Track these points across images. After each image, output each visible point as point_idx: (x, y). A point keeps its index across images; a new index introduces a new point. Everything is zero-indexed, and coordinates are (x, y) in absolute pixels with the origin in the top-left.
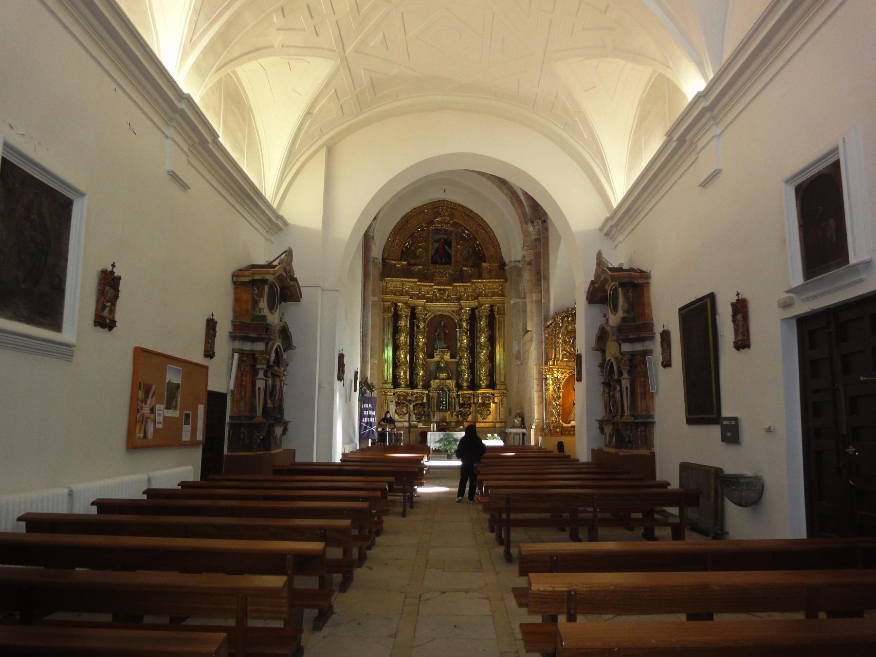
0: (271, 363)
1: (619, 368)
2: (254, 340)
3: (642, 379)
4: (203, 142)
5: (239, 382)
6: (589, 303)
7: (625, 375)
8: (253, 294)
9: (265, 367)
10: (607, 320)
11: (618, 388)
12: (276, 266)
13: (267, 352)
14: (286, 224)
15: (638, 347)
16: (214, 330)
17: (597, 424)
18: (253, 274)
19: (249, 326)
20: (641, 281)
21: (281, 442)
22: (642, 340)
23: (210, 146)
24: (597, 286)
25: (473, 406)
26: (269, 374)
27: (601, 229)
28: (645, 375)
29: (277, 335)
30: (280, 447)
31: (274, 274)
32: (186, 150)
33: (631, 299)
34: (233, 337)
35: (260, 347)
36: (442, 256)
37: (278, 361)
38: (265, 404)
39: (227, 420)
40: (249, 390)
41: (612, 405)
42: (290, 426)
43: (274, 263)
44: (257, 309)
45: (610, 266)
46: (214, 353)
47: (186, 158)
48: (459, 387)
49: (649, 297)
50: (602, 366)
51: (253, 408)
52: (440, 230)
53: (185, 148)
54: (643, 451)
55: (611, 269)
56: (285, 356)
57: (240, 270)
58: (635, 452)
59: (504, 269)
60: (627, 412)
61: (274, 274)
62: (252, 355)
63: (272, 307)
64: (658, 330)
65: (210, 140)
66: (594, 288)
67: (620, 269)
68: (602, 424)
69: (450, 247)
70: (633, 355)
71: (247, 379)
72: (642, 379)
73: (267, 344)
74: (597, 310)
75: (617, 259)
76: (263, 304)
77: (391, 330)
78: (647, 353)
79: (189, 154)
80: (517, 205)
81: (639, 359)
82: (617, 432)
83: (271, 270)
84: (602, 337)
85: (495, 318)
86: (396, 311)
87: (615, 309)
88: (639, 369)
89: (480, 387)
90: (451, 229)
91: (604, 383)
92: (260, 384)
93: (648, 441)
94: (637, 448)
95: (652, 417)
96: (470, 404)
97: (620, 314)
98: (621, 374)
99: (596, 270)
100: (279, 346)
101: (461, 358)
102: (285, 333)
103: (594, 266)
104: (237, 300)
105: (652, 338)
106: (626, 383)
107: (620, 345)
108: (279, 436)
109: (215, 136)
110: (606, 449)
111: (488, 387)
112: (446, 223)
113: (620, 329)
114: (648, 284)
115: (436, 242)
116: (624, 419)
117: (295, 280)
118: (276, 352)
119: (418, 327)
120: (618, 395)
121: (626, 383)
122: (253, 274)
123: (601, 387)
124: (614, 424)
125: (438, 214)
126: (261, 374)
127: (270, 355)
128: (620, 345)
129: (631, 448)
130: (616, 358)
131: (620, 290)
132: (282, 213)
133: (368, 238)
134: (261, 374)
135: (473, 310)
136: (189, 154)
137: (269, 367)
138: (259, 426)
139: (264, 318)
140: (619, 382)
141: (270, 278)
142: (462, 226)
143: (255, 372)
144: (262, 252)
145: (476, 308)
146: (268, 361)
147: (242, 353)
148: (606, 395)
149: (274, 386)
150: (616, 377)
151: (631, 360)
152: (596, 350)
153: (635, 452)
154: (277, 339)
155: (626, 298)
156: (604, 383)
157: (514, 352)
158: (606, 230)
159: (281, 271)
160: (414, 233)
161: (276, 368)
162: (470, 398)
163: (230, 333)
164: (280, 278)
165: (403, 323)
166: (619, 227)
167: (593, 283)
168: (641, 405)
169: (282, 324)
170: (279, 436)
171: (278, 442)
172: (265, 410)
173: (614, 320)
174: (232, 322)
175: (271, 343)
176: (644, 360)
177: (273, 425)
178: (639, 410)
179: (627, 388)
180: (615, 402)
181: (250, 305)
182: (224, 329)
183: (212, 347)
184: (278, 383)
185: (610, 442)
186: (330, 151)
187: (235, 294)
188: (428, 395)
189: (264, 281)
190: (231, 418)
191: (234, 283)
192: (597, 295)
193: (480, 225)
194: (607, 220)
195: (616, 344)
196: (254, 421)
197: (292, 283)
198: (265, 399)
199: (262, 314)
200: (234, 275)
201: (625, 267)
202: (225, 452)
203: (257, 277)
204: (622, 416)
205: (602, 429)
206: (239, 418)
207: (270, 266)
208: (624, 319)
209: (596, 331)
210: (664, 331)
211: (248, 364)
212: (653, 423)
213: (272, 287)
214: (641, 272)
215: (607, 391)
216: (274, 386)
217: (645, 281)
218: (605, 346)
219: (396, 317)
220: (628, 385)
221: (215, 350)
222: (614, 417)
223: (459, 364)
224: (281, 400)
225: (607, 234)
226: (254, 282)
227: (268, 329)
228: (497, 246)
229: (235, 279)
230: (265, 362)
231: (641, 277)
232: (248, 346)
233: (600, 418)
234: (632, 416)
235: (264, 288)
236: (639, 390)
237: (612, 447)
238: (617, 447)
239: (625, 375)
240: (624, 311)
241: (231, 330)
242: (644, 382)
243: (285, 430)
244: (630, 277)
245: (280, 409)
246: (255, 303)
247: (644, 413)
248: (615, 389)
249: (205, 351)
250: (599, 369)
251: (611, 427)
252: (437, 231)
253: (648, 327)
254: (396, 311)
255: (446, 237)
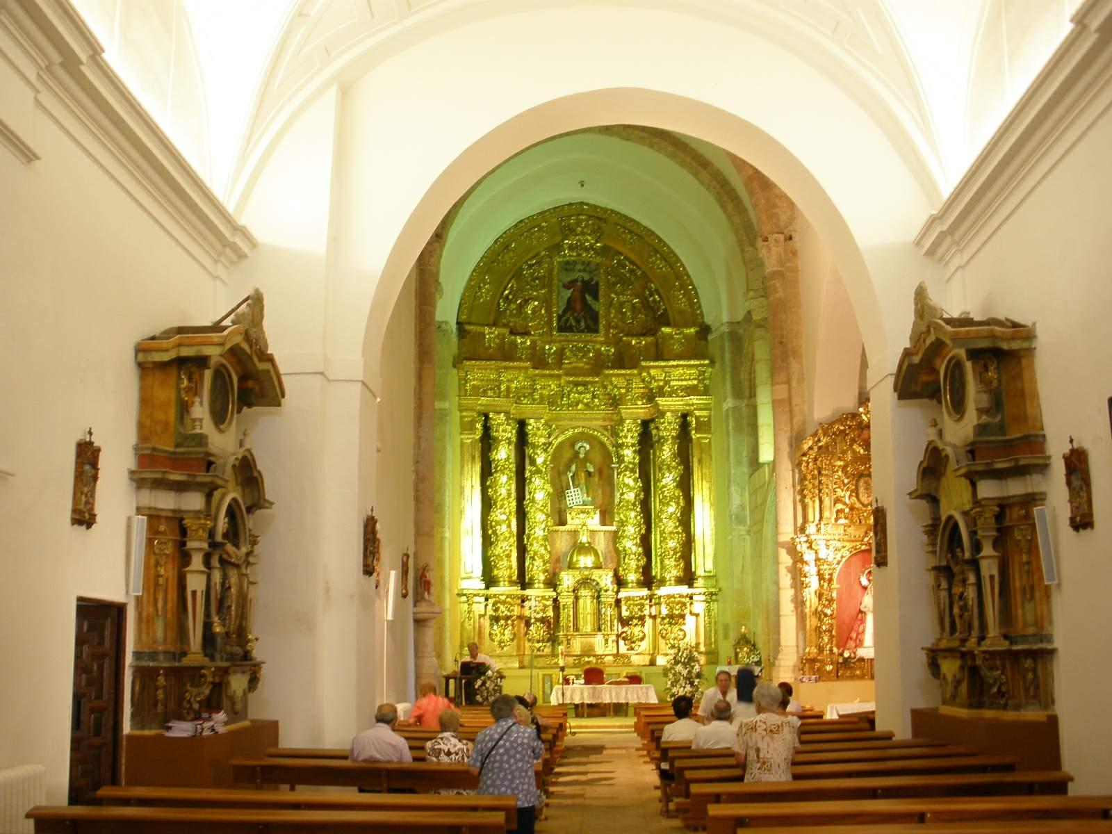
0: (219, 538)
1: (973, 533)
2: (180, 487)
3: (1025, 558)
4: (70, 63)
5: (152, 582)
6: (900, 398)
7: (988, 550)
8: (179, 390)
9: (205, 545)
10: (940, 434)
11: (972, 579)
12: (225, 328)
13: (208, 513)
14: (253, 244)
15: (1015, 488)
16: (95, 465)
17: (922, 657)
18: (180, 345)
19: (169, 461)
20: (1015, 345)
21: (246, 707)
22: (1020, 471)
23: (84, 69)
24: (916, 359)
25: (649, 622)
26: (215, 562)
27: (918, 243)
28: (1032, 547)
29: (229, 473)
30: (245, 717)
31: (222, 344)
32: (33, 78)
33: (995, 384)
34: (139, 481)
35: (194, 501)
36: (580, 314)
37: (234, 534)
38: (208, 626)
39: (129, 659)
40: (173, 595)
41: (955, 618)
42: (265, 671)
43: (224, 323)
44: (187, 421)
45: (945, 316)
46: (93, 516)
47: (30, 94)
48: (620, 582)
49: (1033, 380)
50: (932, 530)
51: (182, 632)
52: (575, 262)
53: (31, 73)
54: (1032, 714)
55: (949, 321)
56: (250, 522)
57: (153, 338)
58: (1009, 715)
59: (706, 339)
60: (993, 631)
61: (222, 344)
62: (180, 524)
63: (219, 417)
64: (1057, 449)
65: (83, 57)
66: (911, 366)
67: (966, 321)
68: (934, 657)
69: (596, 297)
70: (1003, 506)
71: (168, 572)
72: (1025, 558)
73: (209, 496)
74: (915, 413)
75: (958, 300)
76: (201, 410)
77: (477, 468)
78: (1032, 500)
79: (39, 86)
80: (730, 206)
81: (1015, 513)
82: (972, 672)
83: (215, 337)
84: (933, 466)
85: (690, 440)
86: (487, 428)
87: (958, 407)
88: (1017, 535)
89: (662, 582)
90: (598, 260)
91: (937, 569)
92: (196, 583)
93: (1041, 693)
94: (1017, 708)
95: (1049, 639)
96: (642, 618)
97: (971, 417)
98: (977, 547)
99: (915, 324)
100: (234, 500)
101: (622, 523)
102: (248, 473)
103: (910, 317)
104: (145, 401)
105: (1043, 468)
106: (989, 568)
107: (974, 485)
108: (239, 693)
109: (95, 51)
110: (946, 710)
111: (679, 581)
112: (587, 249)
113: (972, 451)
114: (1030, 352)
115: (566, 287)
116: (987, 646)
117: (270, 359)
118: (232, 513)
119: (533, 462)
120: (971, 593)
121: (989, 568)
122: (180, 345)
123: (930, 578)
124: (963, 655)
125: (569, 231)
126: (197, 562)
127: (215, 519)
128: (974, 485)
129: (1005, 707)
130: (965, 513)
131: (969, 365)
132: (243, 220)
133: (425, 277)
134: (197, 562)
135: (645, 424)
136: (39, 86)
137: (214, 545)
138: (194, 673)
139: (201, 439)
140: (974, 564)
141: (213, 352)
142: (620, 253)
143: (184, 557)
144: (207, 302)
145: (652, 420)
146: (212, 534)
147: (154, 517)
148: (944, 594)
149: (225, 588)
150: (967, 555)
151: (999, 517)
152: (921, 497)
153: (1009, 715)
154: (231, 485)
155: (981, 379)
156: (937, 569)
157: (734, 509)
158: (927, 244)
159: (238, 339)
160: (521, 269)
161: (230, 547)
162: (642, 605)
163: (132, 473)
164: (235, 352)
165: (503, 453)
166: (958, 235)
167: (907, 354)
168: (1024, 613)
169: (241, 453)
170: (239, 693)
171: (239, 707)
172: (209, 638)
173: (958, 432)
174: (137, 448)
175: (217, 494)
176: (1028, 516)
177: (225, 672)
178: (1020, 625)
179: (992, 577)
180: (964, 608)
181: (172, 414)
182: (117, 463)
183: (90, 503)
184: (233, 579)
185: (954, 697)
186: (345, 93)
187: (143, 388)
188: (555, 600)
189: (201, 362)
190: (138, 655)
191: (141, 366)
192: (922, 377)
193: (656, 251)
194: (933, 221)
195: (965, 483)
196: (185, 662)
197: (262, 366)
198: (208, 614)
199: (198, 431)
200: (140, 349)
201: (977, 317)
202: (127, 728)
203: (187, 352)
204: (982, 638)
205: (934, 666)
206: (153, 655)
207: (217, 327)
208: (981, 429)
209: (918, 456)
210: (1073, 451)
211: (169, 537)
212: (1052, 652)
213: (220, 376)
214: (1015, 325)
215: (944, 585)
216: (225, 588)
217: (1025, 345)
218: (937, 489)
219: (488, 442)
220: (995, 572)
221: (96, 511)
222: (964, 641)
223: (615, 537)
224: (243, 615)
225: (931, 252)
226: (180, 362)
227: (210, 464)
228: (692, 296)
229: (141, 357)
230: (205, 535)
231: (1013, 338)
232: (166, 501)
233: (928, 644)
234: (1006, 637)
235: (202, 376)
236: (1017, 582)
237: (962, 706)
238: (971, 706)
239: (988, 550)
240: (981, 411)
241: (133, 466)
242: (1029, 563)
243: (254, 681)
244: (993, 336)
245: (241, 634)
246: (184, 408)
247: (1031, 630)
248: (964, 581)
249: (75, 511)
250: (925, 538)
251: (958, 663)
252: (568, 266)
253: (1035, 442)
254: (487, 428)
255: (587, 277)
